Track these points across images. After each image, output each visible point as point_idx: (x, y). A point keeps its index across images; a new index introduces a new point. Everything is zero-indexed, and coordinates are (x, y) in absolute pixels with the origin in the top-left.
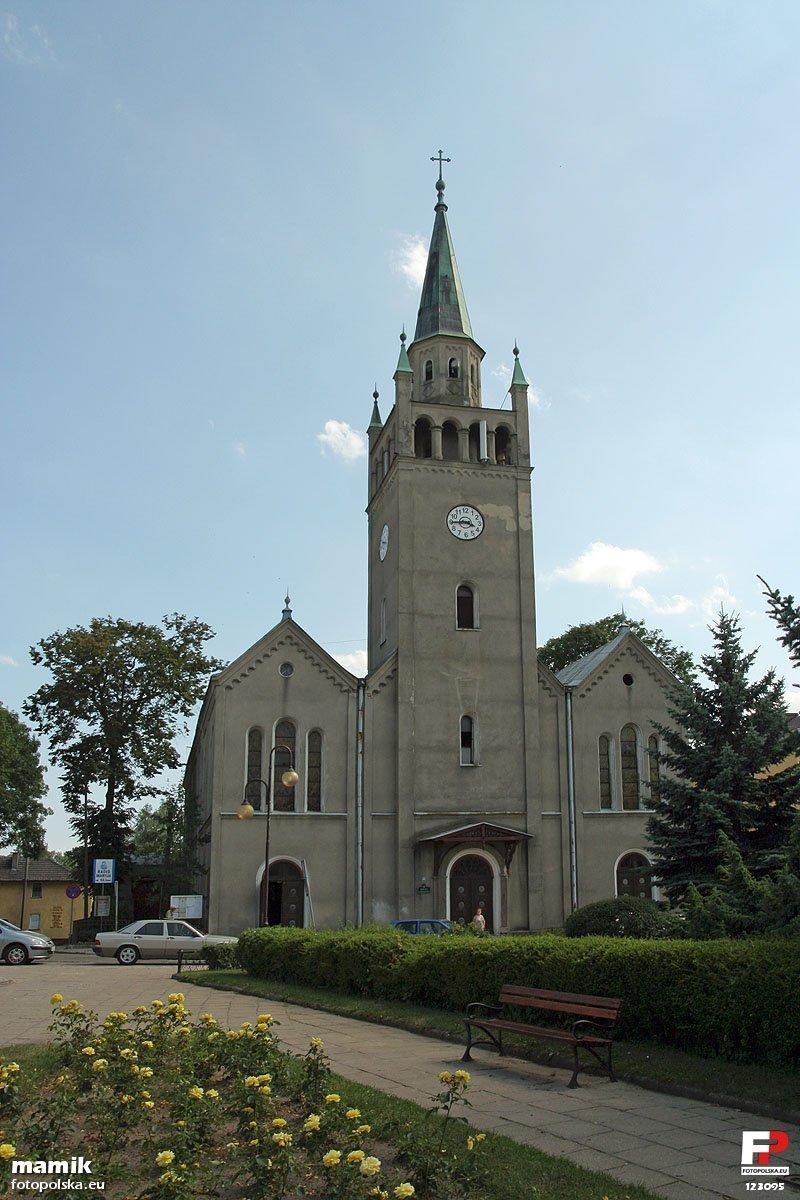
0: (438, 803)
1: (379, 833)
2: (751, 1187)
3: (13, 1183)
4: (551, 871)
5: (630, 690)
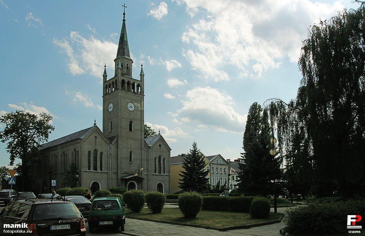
0: (126, 170)
1: (114, 176)
2: (350, 232)
3: (4, 231)
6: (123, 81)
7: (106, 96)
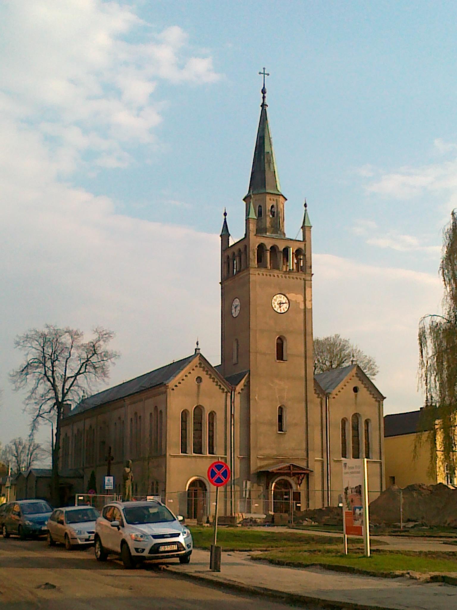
0: (267, 452)
4: (318, 487)
5: (356, 396)
6: (261, 247)
7: (226, 283)
